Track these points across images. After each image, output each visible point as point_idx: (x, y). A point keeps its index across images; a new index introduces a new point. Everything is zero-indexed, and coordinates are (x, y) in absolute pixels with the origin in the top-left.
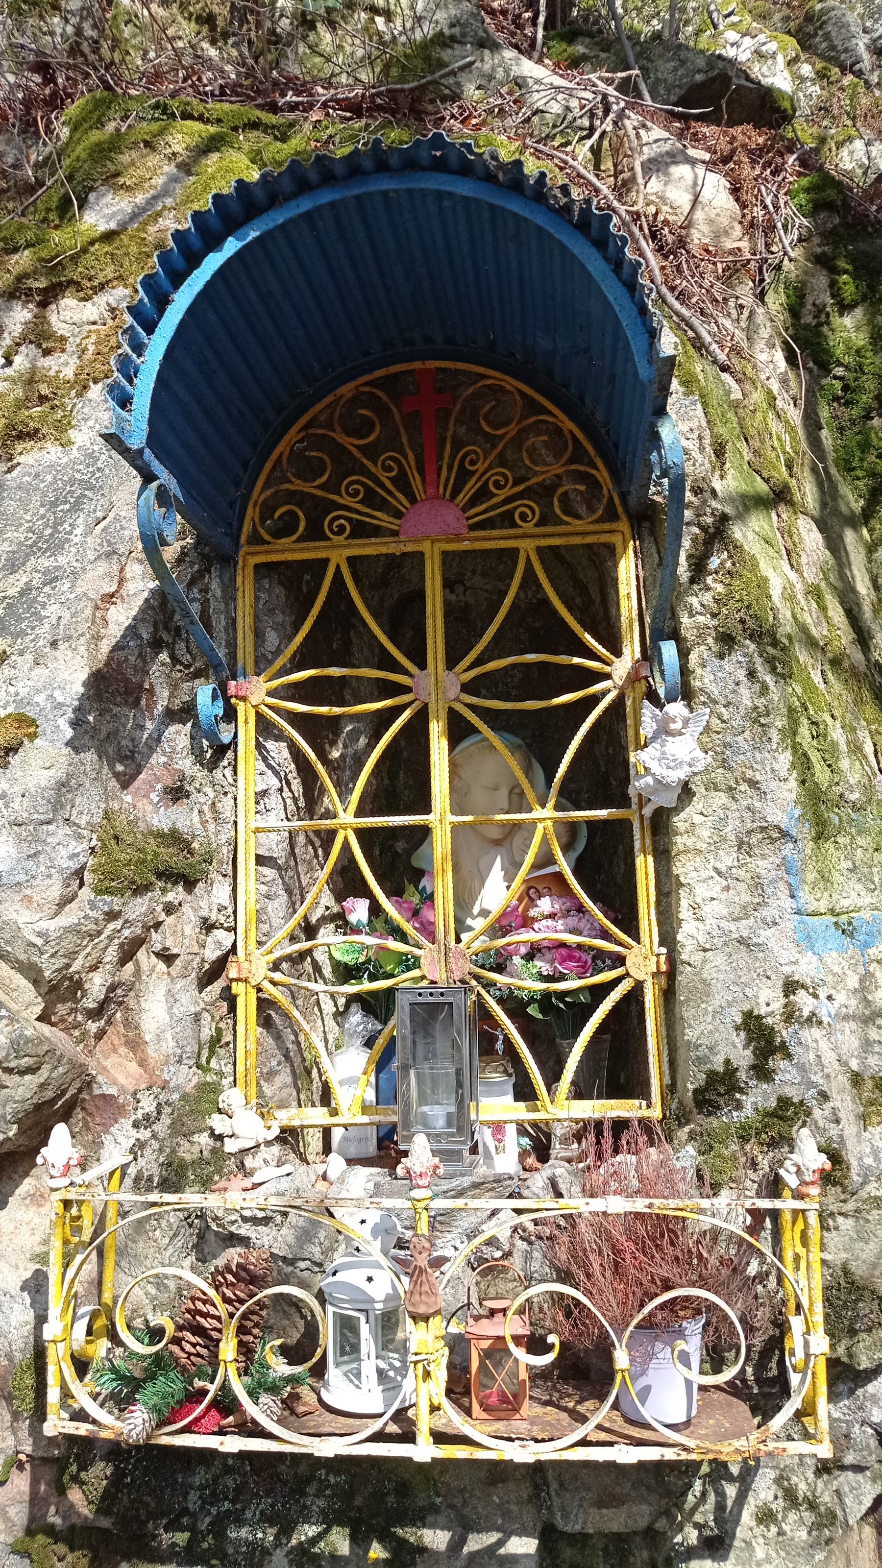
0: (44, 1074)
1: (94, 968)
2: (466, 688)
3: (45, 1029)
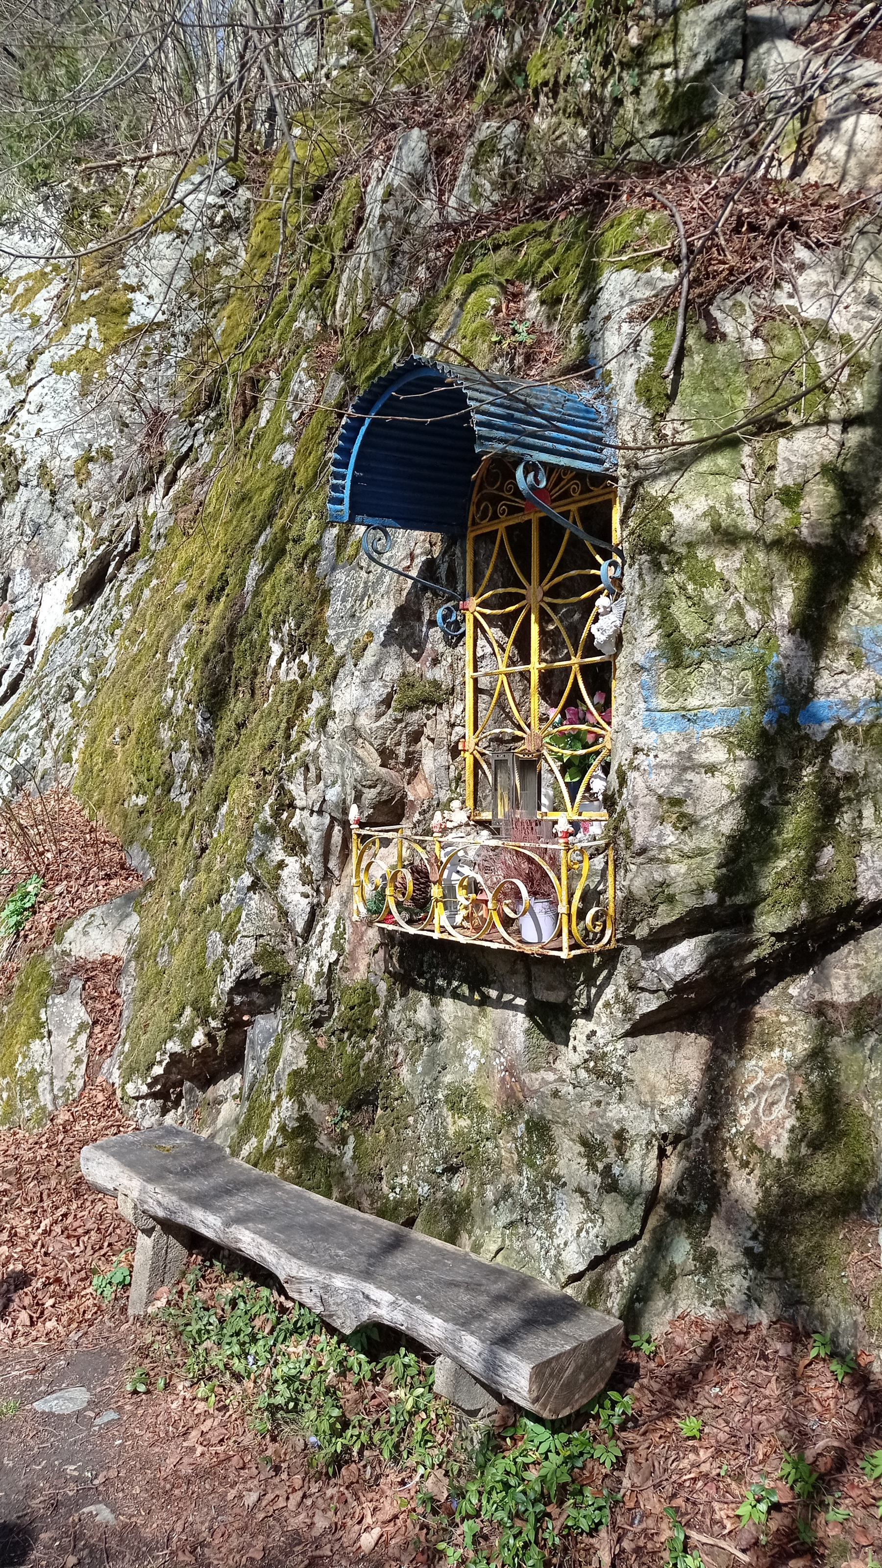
0: (379, 788)
1: (398, 744)
2: (546, 594)
3: (384, 770)
